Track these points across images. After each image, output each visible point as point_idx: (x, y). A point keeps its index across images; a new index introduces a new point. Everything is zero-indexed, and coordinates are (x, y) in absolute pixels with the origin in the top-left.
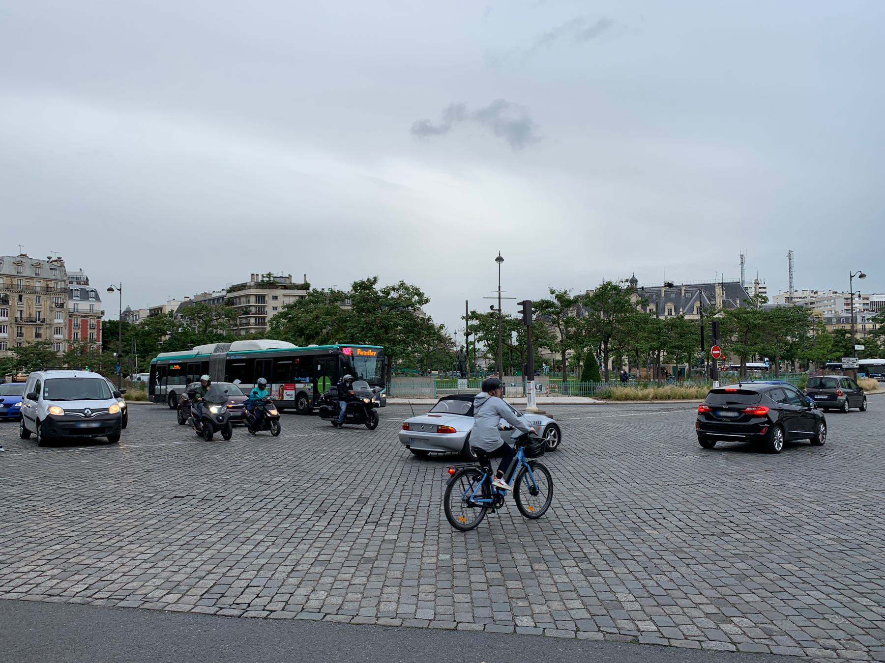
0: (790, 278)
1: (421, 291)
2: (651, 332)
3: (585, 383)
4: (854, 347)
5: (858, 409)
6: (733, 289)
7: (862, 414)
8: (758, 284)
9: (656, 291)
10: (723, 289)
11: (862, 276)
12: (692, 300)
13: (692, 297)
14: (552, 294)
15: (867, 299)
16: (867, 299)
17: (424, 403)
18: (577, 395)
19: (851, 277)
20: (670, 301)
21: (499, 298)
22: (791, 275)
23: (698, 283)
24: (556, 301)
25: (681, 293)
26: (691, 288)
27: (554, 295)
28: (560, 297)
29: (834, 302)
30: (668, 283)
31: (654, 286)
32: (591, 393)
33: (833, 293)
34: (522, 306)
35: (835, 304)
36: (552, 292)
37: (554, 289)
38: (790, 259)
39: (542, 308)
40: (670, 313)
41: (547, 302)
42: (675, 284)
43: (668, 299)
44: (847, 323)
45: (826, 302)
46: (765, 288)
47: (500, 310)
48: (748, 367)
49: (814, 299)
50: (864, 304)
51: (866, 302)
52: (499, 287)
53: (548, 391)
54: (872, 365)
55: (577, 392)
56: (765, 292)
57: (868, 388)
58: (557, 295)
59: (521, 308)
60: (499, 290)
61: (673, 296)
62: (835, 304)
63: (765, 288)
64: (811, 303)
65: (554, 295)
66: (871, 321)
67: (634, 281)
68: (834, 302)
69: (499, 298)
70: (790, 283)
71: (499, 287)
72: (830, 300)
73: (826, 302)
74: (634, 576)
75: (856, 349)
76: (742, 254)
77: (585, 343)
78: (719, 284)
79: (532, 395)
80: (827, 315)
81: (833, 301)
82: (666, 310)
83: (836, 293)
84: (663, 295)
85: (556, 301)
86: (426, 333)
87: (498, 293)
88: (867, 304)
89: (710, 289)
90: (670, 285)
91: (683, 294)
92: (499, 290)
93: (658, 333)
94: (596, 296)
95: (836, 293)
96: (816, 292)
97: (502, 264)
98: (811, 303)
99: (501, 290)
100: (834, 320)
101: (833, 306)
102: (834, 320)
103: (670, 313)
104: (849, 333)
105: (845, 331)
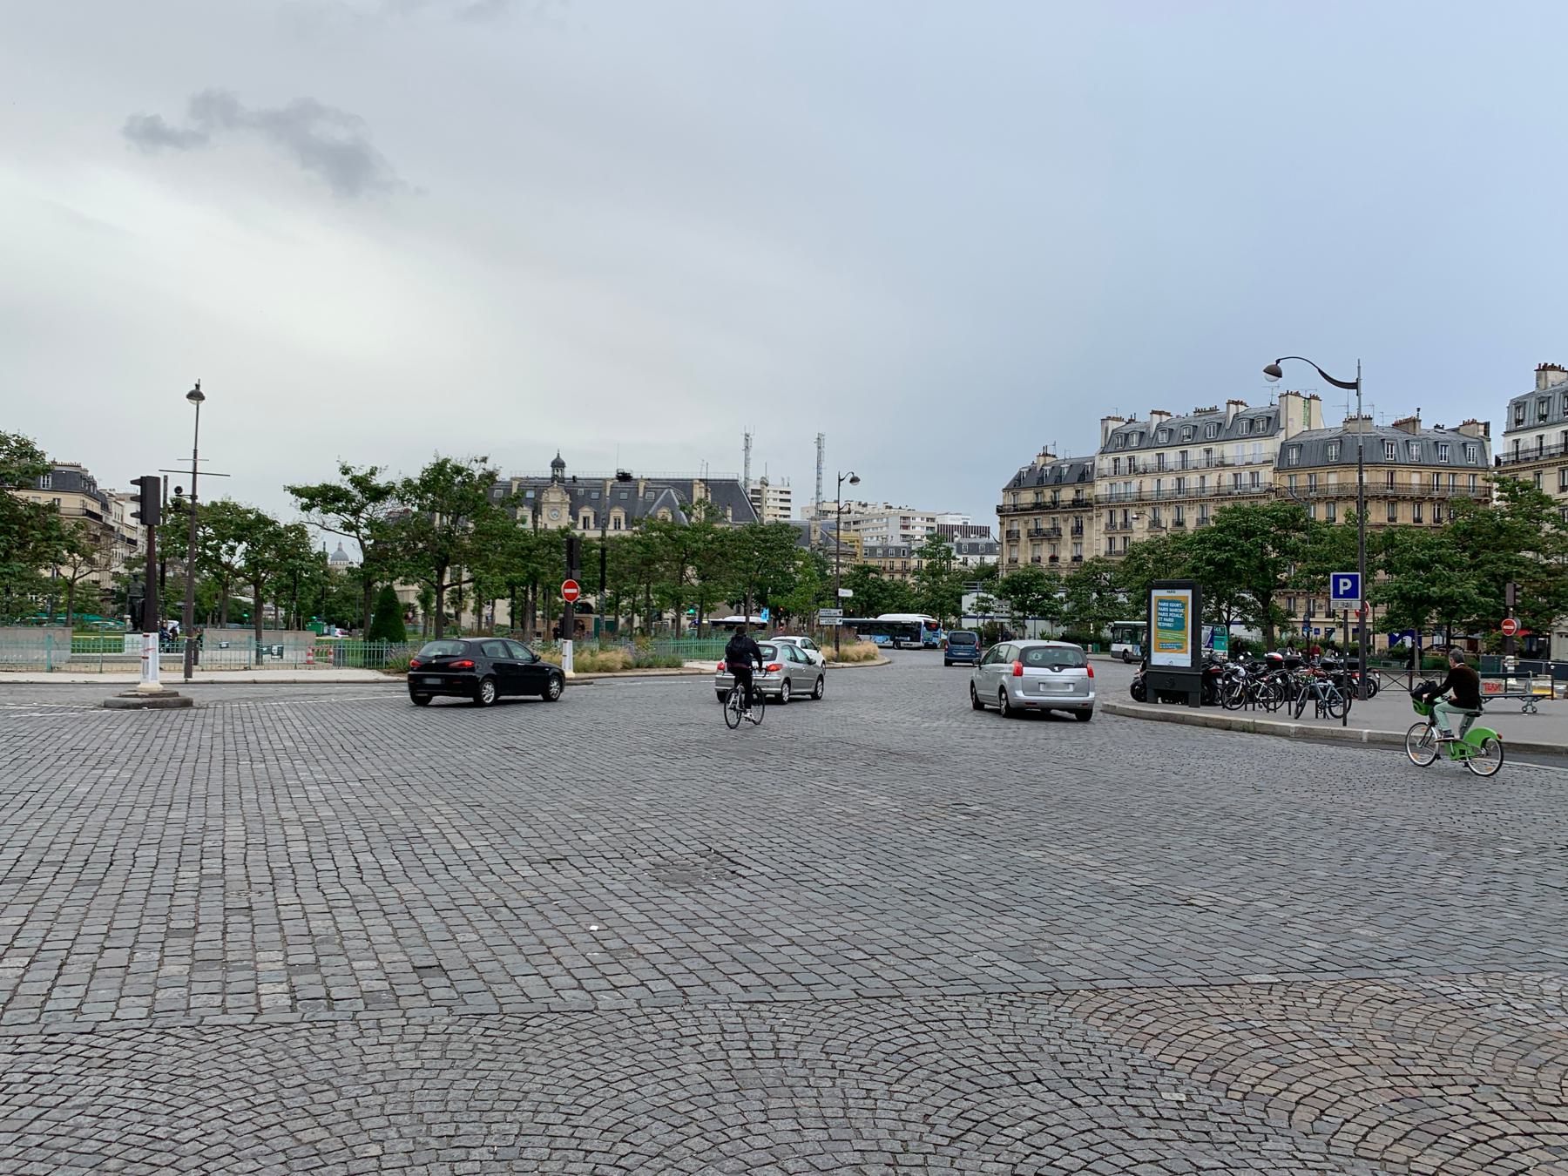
0: (818, 479)
1: (38, 448)
2: (513, 555)
3: (372, 644)
4: (837, 593)
5: (540, 697)
6: (725, 491)
7: (816, 703)
8: (767, 485)
9: (598, 485)
10: (707, 490)
11: (854, 480)
12: (655, 506)
13: (655, 500)
14: (344, 473)
15: (933, 520)
16: (933, 520)
17: (11, 680)
18: (357, 667)
19: (840, 480)
20: (619, 505)
21: (195, 473)
22: (819, 473)
23: (671, 477)
24: (350, 487)
25: (638, 492)
26: (657, 485)
27: (347, 477)
28: (357, 482)
29: (887, 522)
30: (623, 474)
31: (594, 477)
32: (382, 663)
33: (887, 507)
34: (139, 487)
35: (887, 526)
36: (345, 471)
37: (348, 465)
38: (819, 448)
39: (324, 500)
40: (617, 526)
41: (336, 489)
42: (635, 476)
43: (616, 502)
44: (897, 556)
45: (875, 521)
46: (788, 493)
47: (194, 497)
48: (753, 623)
49: (858, 515)
50: (928, 528)
51: (930, 524)
52: (195, 451)
53: (311, 658)
54: (899, 623)
55: (360, 660)
56: (789, 501)
57: (856, 658)
58: (355, 477)
59: (136, 490)
60: (195, 457)
61: (624, 496)
62: (887, 526)
63: (788, 493)
64: (855, 523)
65: (347, 477)
66: (916, 555)
67: (558, 464)
68: (887, 522)
69: (195, 473)
70: (818, 486)
71: (195, 451)
72: (882, 519)
73: (875, 521)
74: (672, 982)
75: (840, 595)
76: (748, 432)
77: (397, 570)
78: (701, 480)
79: (150, 660)
80: (873, 543)
81: (885, 520)
82: (612, 520)
83: (891, 508)
84: (608, 494)
85: (350, 487)
86: (39, 536)
87: (192, 462)
88: (932, 528)
89: (685, 486)
90: (624, 477)
91: (641, 494)
92: (195, 457)
93: (527, 558)
94: (424, 482)
95: (891, 508)
96: (865, 505)
97: (202, 404)
98: (855, 523)
99: (198, 457)
100: (880, 551)
101: (885, 529)
102: (880, 551)
103: (617, 526)
104: (874, 571)
105: (869, 568)
